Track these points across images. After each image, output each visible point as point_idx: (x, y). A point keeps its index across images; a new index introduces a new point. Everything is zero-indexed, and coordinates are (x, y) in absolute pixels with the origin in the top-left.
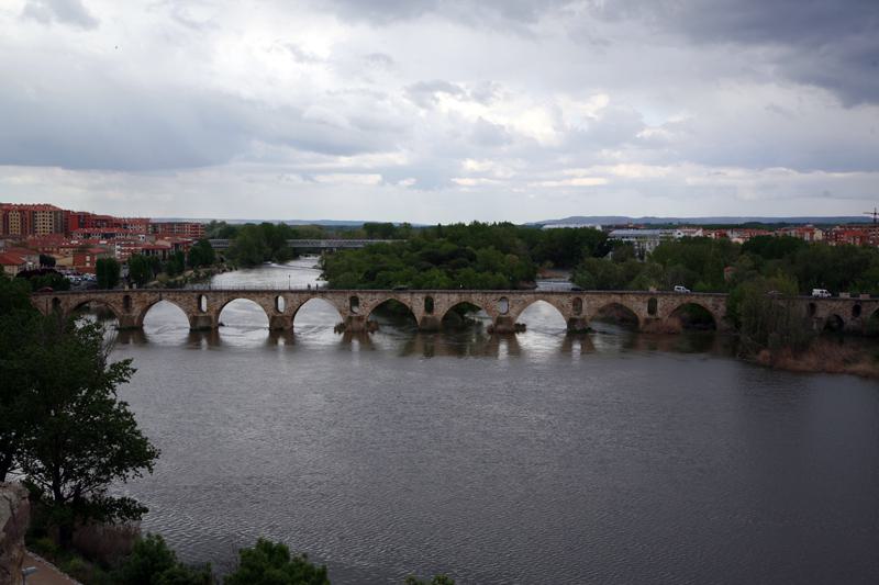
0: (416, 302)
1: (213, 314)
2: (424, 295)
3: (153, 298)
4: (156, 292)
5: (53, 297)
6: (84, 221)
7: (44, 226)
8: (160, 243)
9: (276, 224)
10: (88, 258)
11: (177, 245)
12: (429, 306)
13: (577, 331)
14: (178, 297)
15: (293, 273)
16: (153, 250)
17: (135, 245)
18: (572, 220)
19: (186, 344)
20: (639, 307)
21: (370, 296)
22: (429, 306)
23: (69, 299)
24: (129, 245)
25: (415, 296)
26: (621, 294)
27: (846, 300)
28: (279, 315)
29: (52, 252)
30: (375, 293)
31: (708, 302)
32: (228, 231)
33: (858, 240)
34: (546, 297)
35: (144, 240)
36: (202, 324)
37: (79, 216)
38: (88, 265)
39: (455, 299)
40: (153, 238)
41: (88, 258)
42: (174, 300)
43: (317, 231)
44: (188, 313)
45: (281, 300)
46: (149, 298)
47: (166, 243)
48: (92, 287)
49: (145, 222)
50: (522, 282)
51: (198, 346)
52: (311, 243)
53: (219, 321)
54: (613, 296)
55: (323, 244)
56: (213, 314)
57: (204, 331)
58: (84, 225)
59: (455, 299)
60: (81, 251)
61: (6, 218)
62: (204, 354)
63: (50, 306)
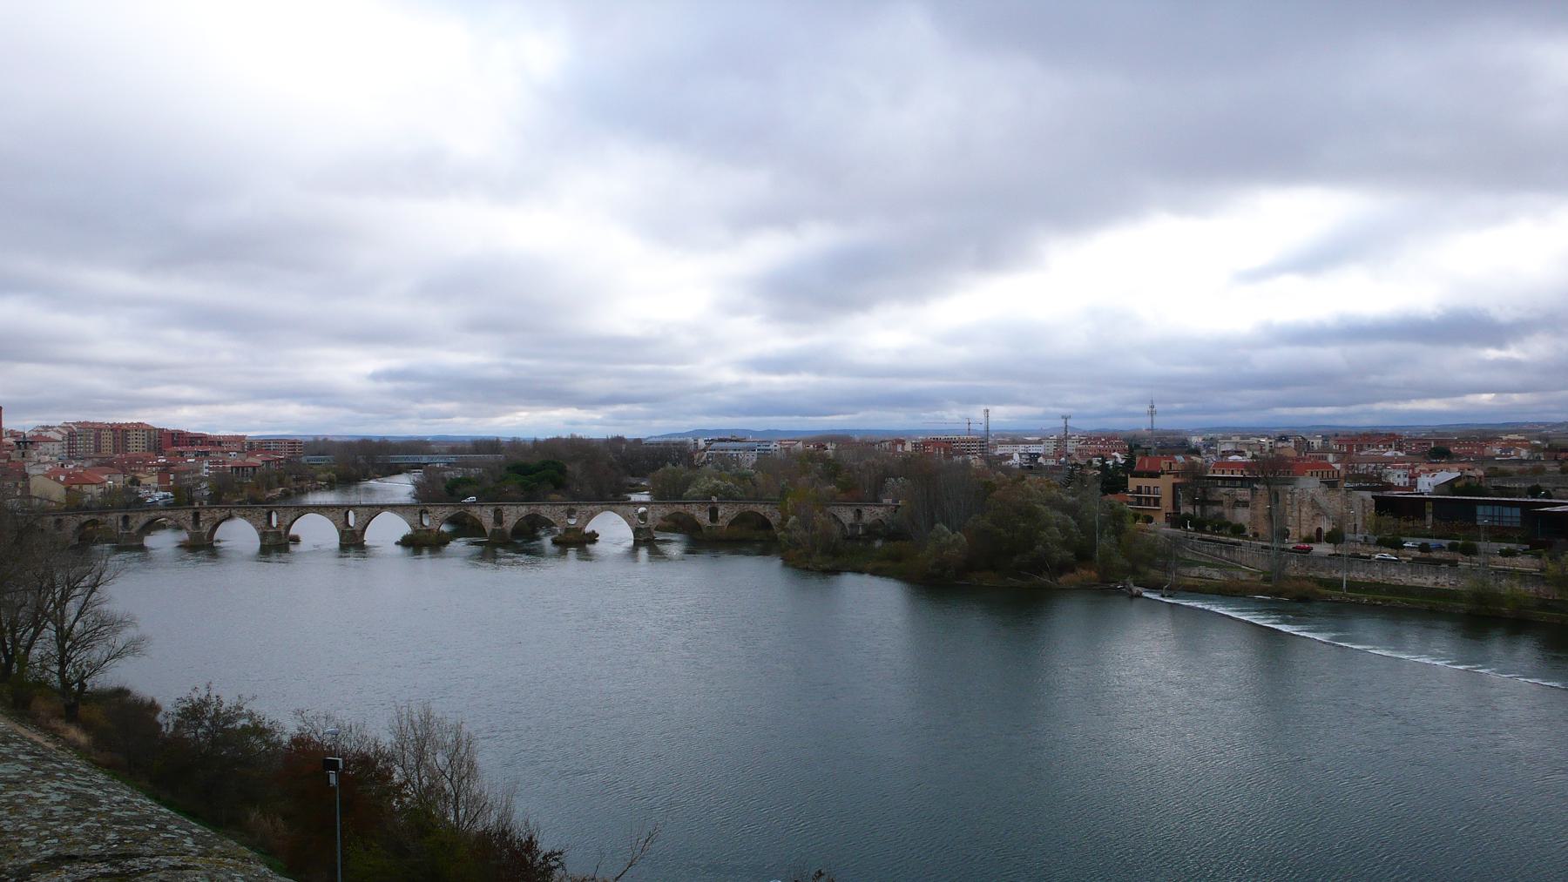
0: (486, 515)
1: (283, 530)
2: (493, 508)
3: (222, 514)
4: (226, 508)
5: (122, 514)
6: (179, 440)
7: (136, 446)
8: (251, 460)
9: (376, 440)
10: (172, 476)
11: (268, 462)
12: (498, 519)
13: (645, 540)
14: (248, 513)
15: (641, 496)
16: (243, 468)
17: (224, 463)
18: (671, 435)
19: (256, 557)
20: (703, 517)
21: (440, 509)
22: (498, 519)
23: (139, 517)
24: (218, 463)
25: (484, 508)
26: (684, 504)
27: (887, 506)
28: (425, 528)
29: (139, 471)
30: (446, 506)
31: (59, 533)
32: (320, 447)
33: (942, 449)
34: (613, 507)
35: (234, 458)
36: (271, 539)
37: (173, 434)
38: (171, 483)
39: (524, 510)
40: (243, 456)
41: (172, 476)
42: (244, 516)
43: (417, 447)
44: (257, 529)
45: (351, 514)
46: (219, 515)
47: (257, 460)
48: (168, 506)
49: (239, 439)
50: (611, 495)
51: (374, 554)
52: (412, 459)
53: (292, 532)
54: (676, 506)
55: (424, 459)
56: (283, 530)
57: (352, 542)
58: (174, 444)
59: (524, 510)
60: (165, 470)
61: (98, 437)
62: (352, 560)
63: (120, 524)
